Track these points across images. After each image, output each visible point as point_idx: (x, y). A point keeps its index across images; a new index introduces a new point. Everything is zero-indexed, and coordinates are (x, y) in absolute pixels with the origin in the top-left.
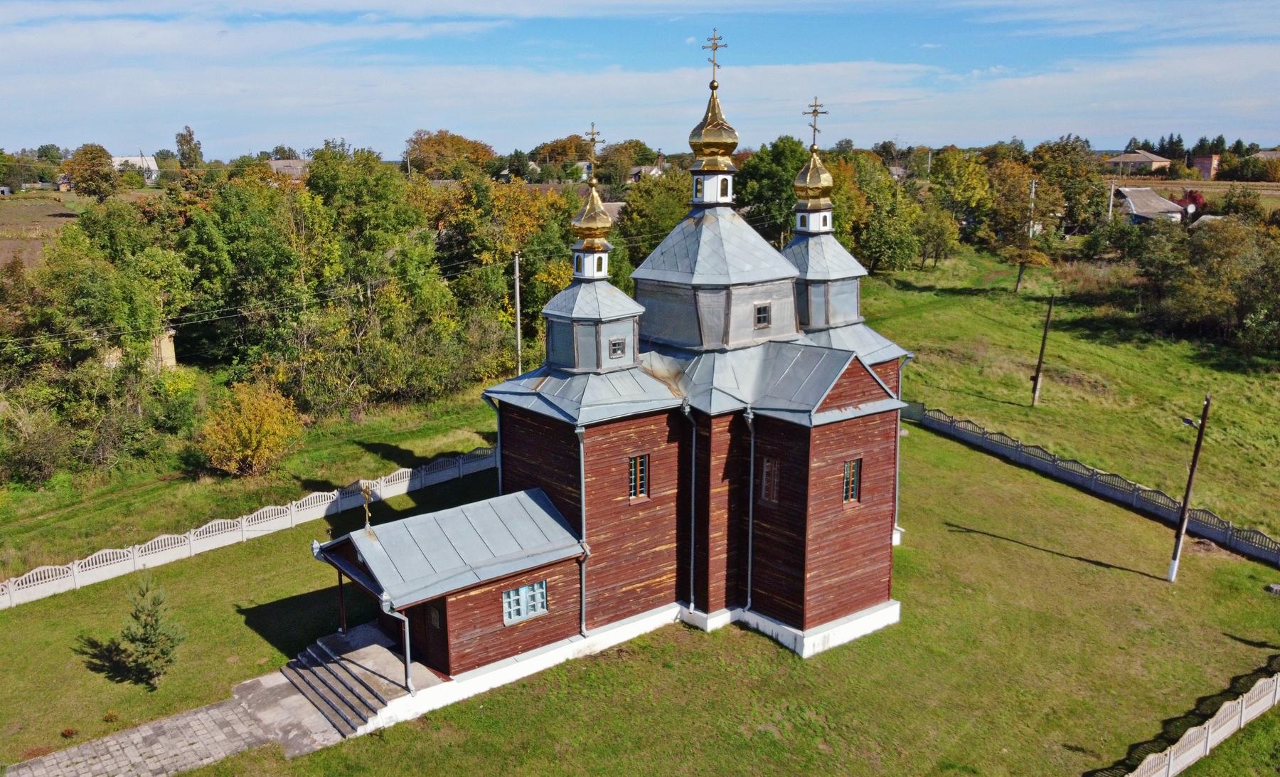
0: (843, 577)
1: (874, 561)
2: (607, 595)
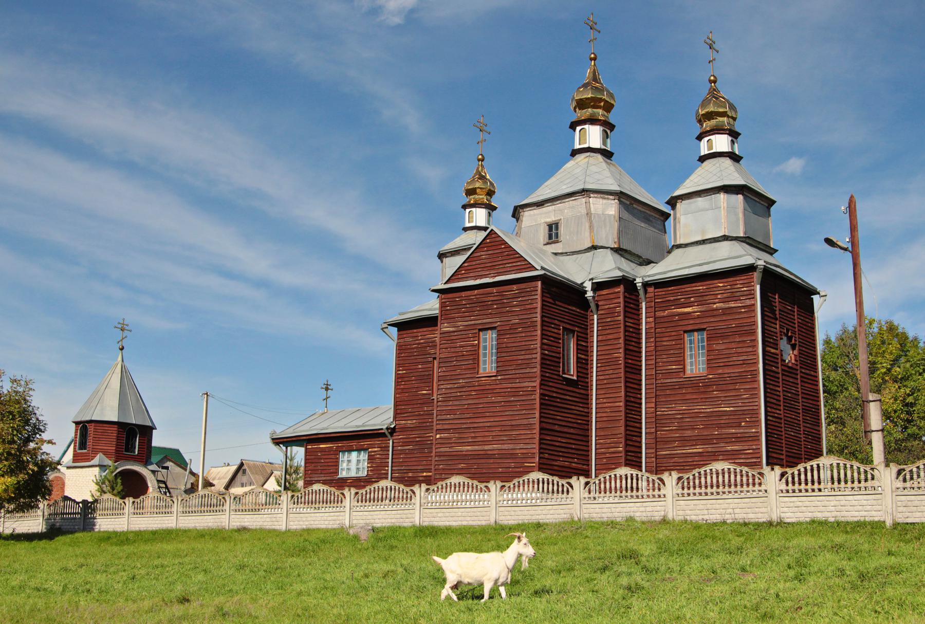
0: (476, 448)
1: (512, 440)
2: (410, 475)
